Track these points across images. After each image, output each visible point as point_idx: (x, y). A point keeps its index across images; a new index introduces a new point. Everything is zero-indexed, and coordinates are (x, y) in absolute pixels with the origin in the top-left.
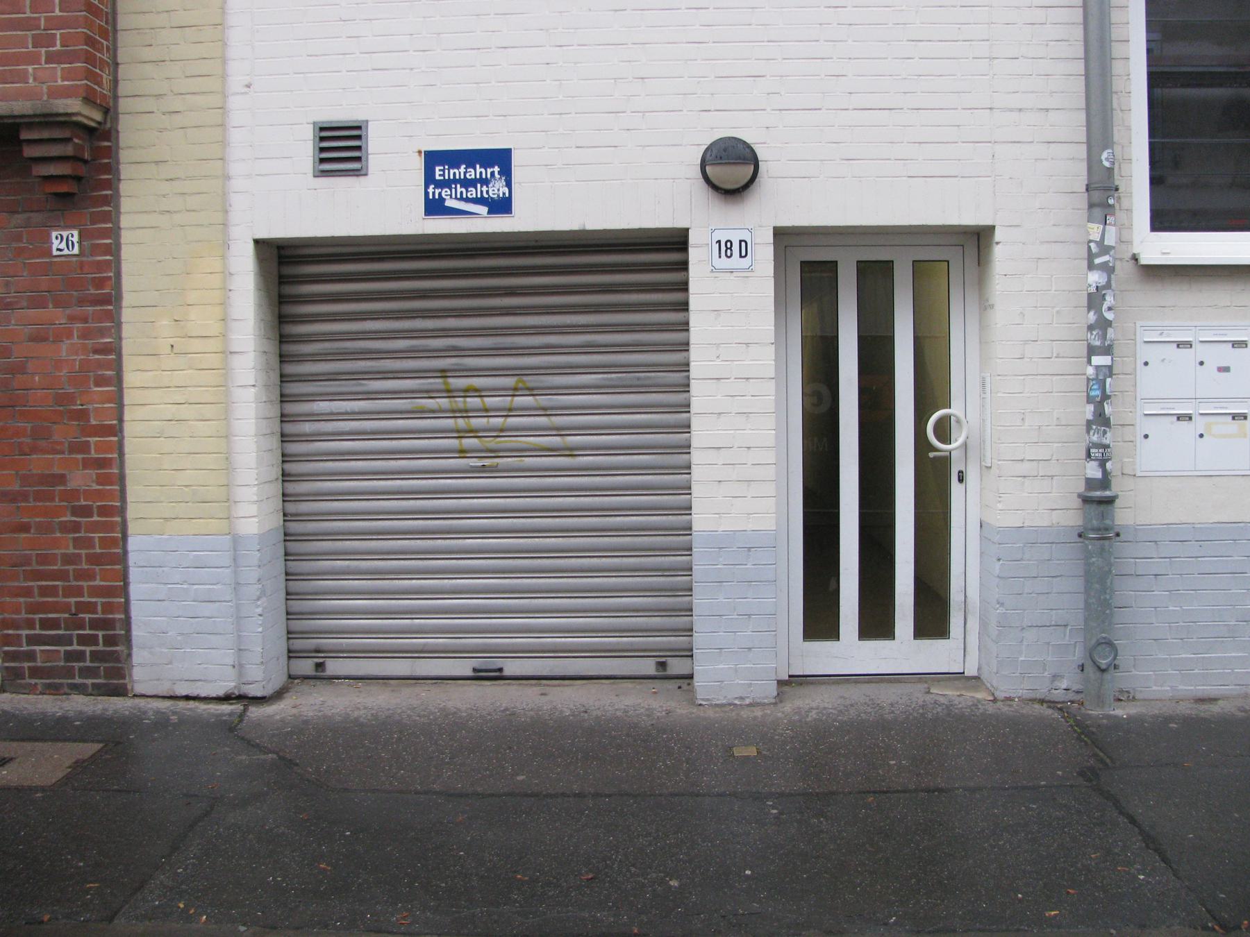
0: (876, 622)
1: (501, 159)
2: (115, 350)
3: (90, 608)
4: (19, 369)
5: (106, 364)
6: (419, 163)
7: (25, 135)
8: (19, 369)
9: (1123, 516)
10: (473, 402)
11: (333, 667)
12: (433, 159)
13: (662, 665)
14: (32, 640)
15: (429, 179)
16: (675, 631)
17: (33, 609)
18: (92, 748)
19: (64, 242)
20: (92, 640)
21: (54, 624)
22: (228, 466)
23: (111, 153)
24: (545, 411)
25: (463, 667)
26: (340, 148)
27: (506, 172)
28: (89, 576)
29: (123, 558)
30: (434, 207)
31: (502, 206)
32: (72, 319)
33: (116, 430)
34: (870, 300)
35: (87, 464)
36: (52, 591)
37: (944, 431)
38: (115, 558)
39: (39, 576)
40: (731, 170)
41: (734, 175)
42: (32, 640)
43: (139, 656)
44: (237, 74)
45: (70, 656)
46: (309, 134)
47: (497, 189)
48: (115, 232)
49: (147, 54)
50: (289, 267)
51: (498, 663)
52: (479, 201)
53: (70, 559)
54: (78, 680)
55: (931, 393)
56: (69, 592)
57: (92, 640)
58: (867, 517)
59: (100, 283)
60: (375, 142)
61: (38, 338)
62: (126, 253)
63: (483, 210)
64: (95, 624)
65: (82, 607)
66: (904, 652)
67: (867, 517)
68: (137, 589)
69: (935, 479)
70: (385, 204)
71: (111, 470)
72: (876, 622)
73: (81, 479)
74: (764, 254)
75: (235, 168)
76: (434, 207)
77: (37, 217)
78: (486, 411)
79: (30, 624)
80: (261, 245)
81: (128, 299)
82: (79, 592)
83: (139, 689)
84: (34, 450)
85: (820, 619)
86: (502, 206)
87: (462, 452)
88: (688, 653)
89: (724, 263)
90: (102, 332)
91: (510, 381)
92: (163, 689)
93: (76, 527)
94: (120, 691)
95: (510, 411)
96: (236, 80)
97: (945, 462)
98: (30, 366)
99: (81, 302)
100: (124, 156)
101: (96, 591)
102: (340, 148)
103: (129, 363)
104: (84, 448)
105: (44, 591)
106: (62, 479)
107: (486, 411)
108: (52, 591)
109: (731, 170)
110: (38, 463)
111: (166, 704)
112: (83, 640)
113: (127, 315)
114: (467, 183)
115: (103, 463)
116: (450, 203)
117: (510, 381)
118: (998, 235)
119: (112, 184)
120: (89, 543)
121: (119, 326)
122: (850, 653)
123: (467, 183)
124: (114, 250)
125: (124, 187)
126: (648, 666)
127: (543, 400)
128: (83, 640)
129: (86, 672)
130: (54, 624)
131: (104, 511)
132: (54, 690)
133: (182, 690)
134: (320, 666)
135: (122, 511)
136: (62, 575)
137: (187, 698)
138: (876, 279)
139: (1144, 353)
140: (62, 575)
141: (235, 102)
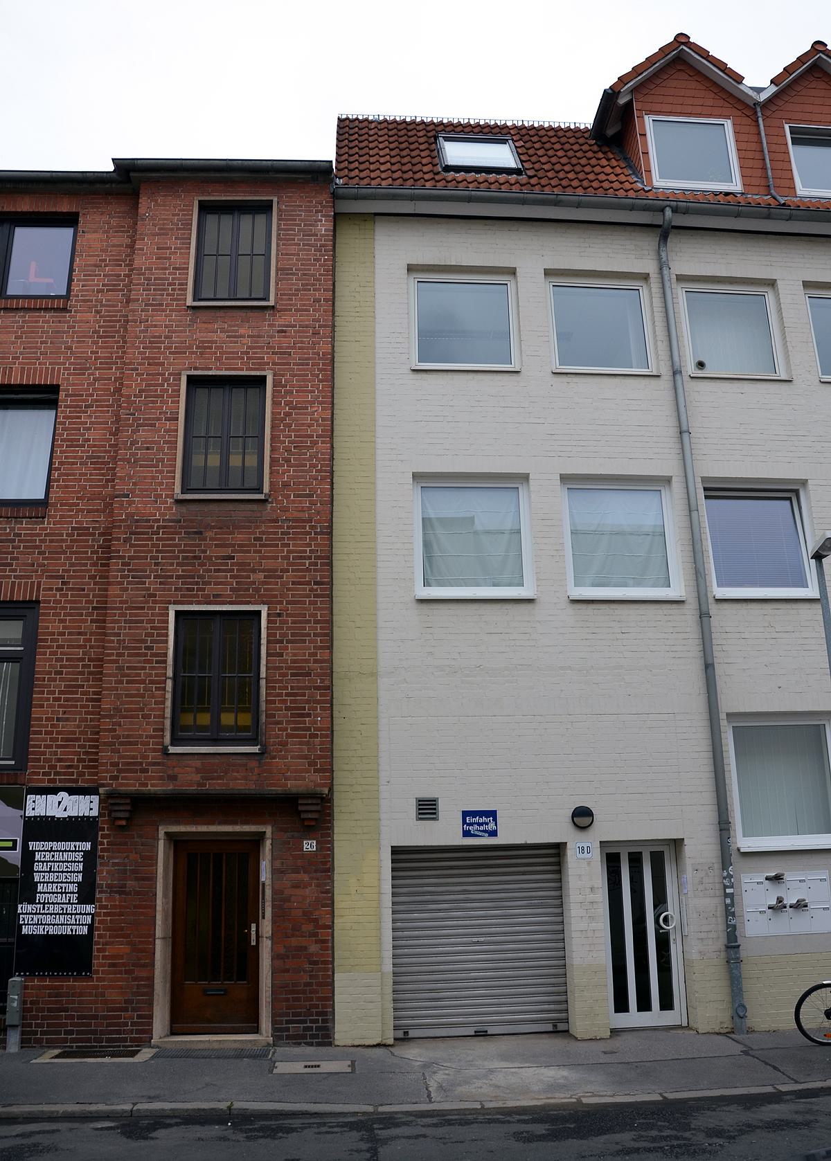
0: (644, 1005)
1: (492, 814)
3: (317, 1006)
4: (288, 900)
5: (327, 899)
8: (288, 900)
9: (743, 953)
11: (412, 1034)
12: (466, 814)
13: (555, 1026)
14: (288, 1022)
15: (464, 822)
16: (560, 1011)
19: (310, 846)
20: (316, 1021)
21: (299, 1014)
22: (380, 943)
23: (331, 808)
25: (471, 1031)
27: (495, 820)
30: (466, 834)
31: (493, 833)
32: (312, 879)
33: (331, 927)
34: (637, 869)
35: (316, 942)
36: (298, 999)
37: (666, 920)
39: (293, 992)
40: (582, 817)
41: (583, 821)
42: (288, 1022)
43: (338, 1027)
44: (384, 776)
45: (305, 1029)
47: (491, 826)
48: (332, 842)
49: (346, 767)
50: (406, 859)
51: (486, 1028)
52: (485, 831)
55: (660, 899)
56: (307, 999)
57: (316, 1021)
58: (642, 969)
59: (325, 863)
60: (441, 806)
61: (296, 886)
64: (318, 1014)
65: (312, 1006)
66: (656, 1017)
67: (642, 969)
69: (663, 943)
70: (446, 831)
71: (327, 944)
72: (644, 1005)
73: (314, 948)
75: (383, 816)
76: (466, 834)
77: (296, 834)
79: (287, 1015)
80: (395, 851)
84: (293, 936)
85: (621, 1005)
86: (493, 833)
88: (567, 1021)
90: (326, 884)
92: (349, 1042)
96: (383, 780)
97: (667, 934)
98: (293, 899)
99: (316, 871)
100: (336, 810)
101: (319, 999)
102: (427, 809)
104: (316, 935)
105: (295, 999)
108: (298, 999)
109: (582, 817)
110: (294, 942)
112: (312, 1021)
114: (479, 824)
118: (686, 842)
119: (331, 821)
120: (317, 977)
121: (333, 882)
122: (634, 1018)
123: (479, 824)
124: (332, 849)
126: (549, 1027)
128: (312, 1021)
129: (312, 1036)
130: (299, 1014)
131: (323, 962)
134: (406, 1033)
135: (333, 962)
136: (304, 992)
138: (636, 860)
139: (744, 887)
140: (304, 992)
141: (382, 788)
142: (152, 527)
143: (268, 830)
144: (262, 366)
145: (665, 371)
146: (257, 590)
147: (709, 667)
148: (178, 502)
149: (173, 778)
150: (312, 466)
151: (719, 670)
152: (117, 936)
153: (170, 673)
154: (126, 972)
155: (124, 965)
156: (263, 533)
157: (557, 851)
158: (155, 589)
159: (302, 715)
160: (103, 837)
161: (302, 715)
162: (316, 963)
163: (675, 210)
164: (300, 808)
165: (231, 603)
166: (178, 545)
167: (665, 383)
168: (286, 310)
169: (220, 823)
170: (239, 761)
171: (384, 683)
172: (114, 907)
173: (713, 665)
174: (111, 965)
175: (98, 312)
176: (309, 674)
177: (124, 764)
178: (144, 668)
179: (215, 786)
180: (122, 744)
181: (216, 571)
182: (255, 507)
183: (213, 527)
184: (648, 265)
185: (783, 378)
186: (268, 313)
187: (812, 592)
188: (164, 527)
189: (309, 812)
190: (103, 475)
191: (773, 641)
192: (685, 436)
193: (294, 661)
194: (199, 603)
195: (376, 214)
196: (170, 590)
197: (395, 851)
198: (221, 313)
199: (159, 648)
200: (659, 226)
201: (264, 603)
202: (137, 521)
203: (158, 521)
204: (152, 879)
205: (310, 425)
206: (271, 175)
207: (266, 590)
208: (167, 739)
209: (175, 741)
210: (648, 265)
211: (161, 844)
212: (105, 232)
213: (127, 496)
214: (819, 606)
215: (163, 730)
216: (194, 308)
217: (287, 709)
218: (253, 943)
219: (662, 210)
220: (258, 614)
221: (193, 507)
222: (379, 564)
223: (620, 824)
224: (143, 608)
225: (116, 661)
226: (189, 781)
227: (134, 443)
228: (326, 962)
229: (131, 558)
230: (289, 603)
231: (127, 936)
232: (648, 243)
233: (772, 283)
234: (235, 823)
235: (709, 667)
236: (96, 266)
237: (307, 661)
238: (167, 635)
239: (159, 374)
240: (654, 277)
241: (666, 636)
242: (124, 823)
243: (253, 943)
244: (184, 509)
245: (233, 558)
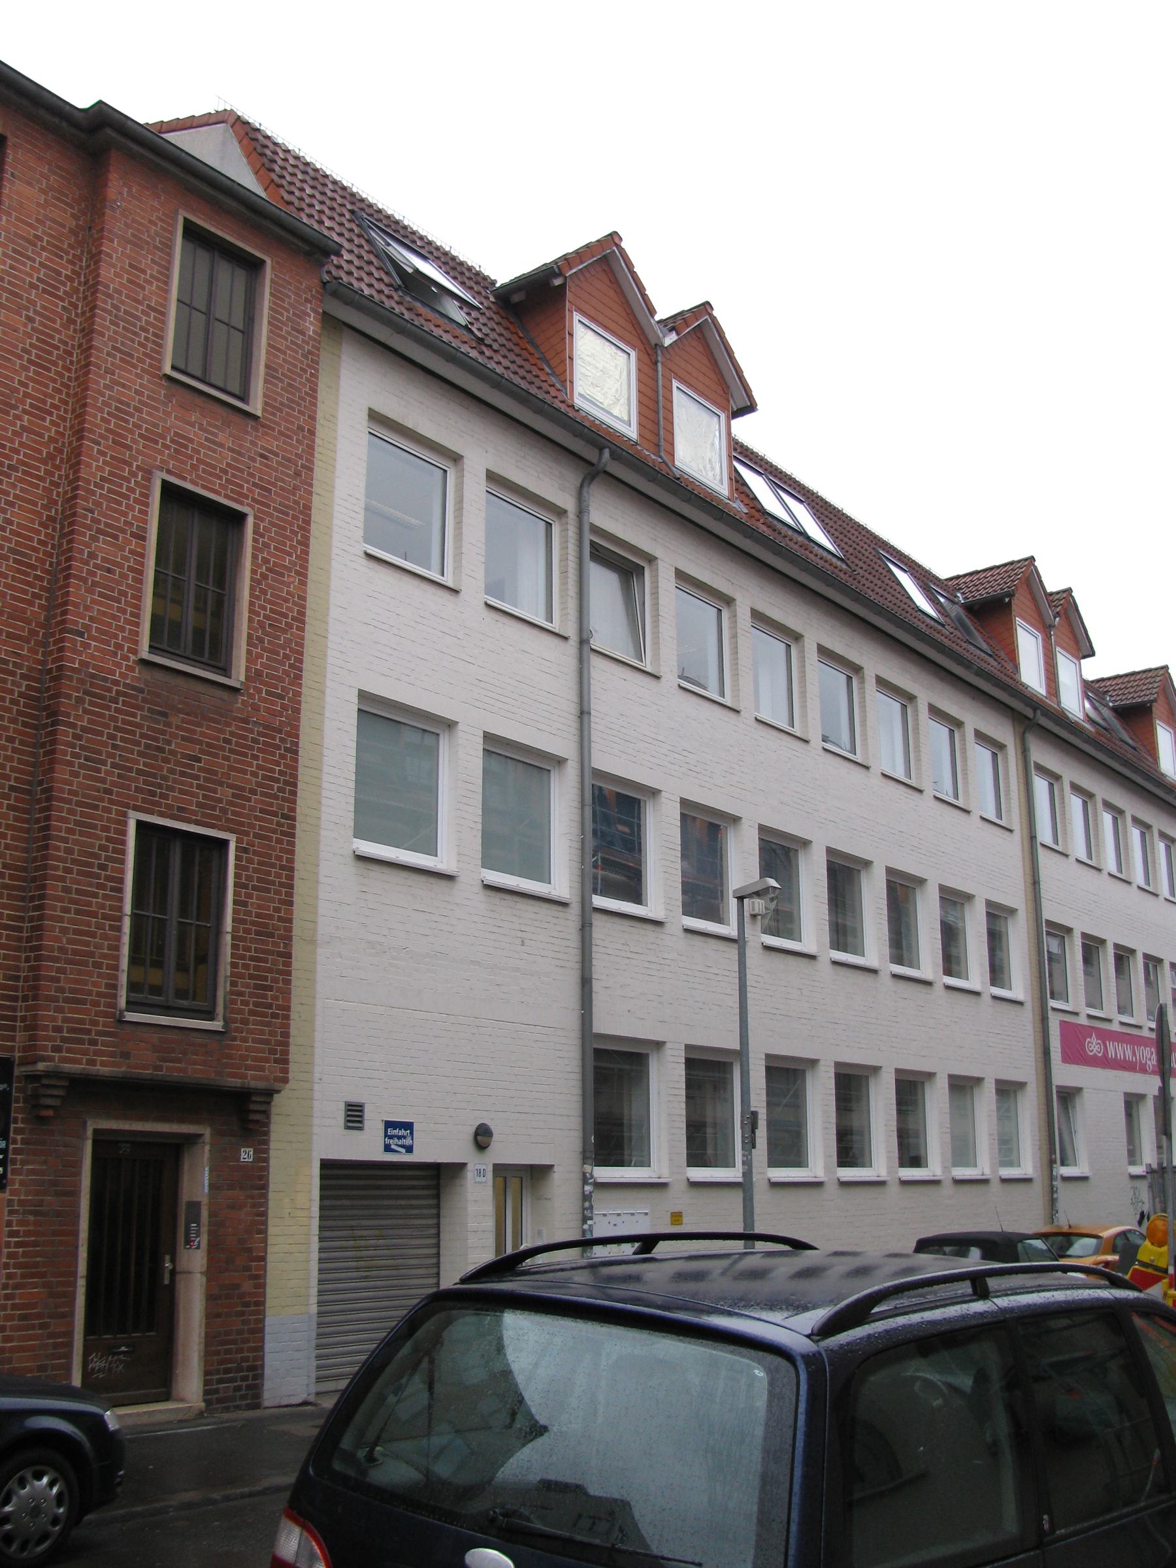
1: (409, 1126)
2: (264, 1214)
6: (382, 1126)
7: (254, 1099)
10: (363, 1243)
12: (389, 1125)
17: (221, 1362)
18: (876, 1310)
19: (246, 1155)
21: (227, 1371)
24: (388, 1247)
26: (354, 1115)
27: (412, 1133)
28: (248, 1341)
29: (262, 1330)
30: (388, 1148)
31: (409, 1149)
33: (263, 1259)
38: (258, 1330)
40: (482, 1137)
43: (268, 1385)
46: (342, 1107)
47: (408, 1142)
50: (336, 1173)
52: (402, 1146)
53: (240, 1332)
54: (238, 1403)
61: (232, 1207)
62: (272, 1162)
63: (403, 1150)
68: (269, 1346)
70: (367, 1146)
71: (259, 1281)
73: (247, 1286)
74: (490, 1175)
76: (388, 1148)
78: (367, 1248)
80: (326, 1165)
81: (272, 1187)
82: (240, 1350)
83: (266, 1403)
87: (357, 1269)
89: (478, 1179)
90: (261, 1205)
91: (376, 1232)
93: (242, 1313)
94: (257, 1406)
95: (376, 1247)
102: (354, 1115)
103: (271, 1222)
104: (248, 1269)
106: (237, 1286)
107: (367, 1248)
109: (482, 1137)
111: (276, 1410)
113: (271, 1195)
114: (399, 1138)
115: (257, 1277)
116: (393, 1147)
117: (376, 1232)
123: (399, 1138)
125: (273, 1127)
127: (388, 1242)
129: (243, 1398)
132: (227, 1409)
133: (285, 1402)
135: (263, 1303)
137: (287, 1406)
142: (109, 690)
143: (206, 1131)
144: (240, 497)
145: (571, 631)
146: (224, 811)
147: (586, 982)
148: (144, 663)
149: (126, 1055)
150: (286, 657)
151: (596, 986)
152: (33, 1276)
153: (128, 908)
154: (41, 1326)
155: (39, 1316)
156: (232, 734)
157: (457, 1169)
158: (113, 784)
159: (265, 988)
160: (18, 1131)
161: (265, 988)
162: (247, 1305)
163: (612, 454)
164: (253, 1107)
165: (197, 823)
166: (140, 726)
167: (571, 647)
168: (270, 428)
169: (117, 1118)
170: (199, 1039)
171: (322, 953)
172: (28, 1234)
173: (591, 979)
174: (23, 1317)
175: (30, 319)
176: (272, 935)
177: (71, 1030)
178: (95, 895)
179: (170, 1071)
180: (66, 1000)
181: (183, 774)
182: (225, 695)
183: (180, 711)
184: (567, 501)
185: (648, 669)
186: (251, 423)
187: (730, 930)
188: (125, 694)
189: (243, 1111)
190: (28, 583)
191: (627, 961)
192: (585, 717)
193: (258, 915)
194: (161, 815)
195: (345, 324)
196: (128, 788)
197: (326, 1165)
198: (199, 400)
199: (114, 869)
200: (593, 465)
201: (232, 831)
202: (93, 676)
203: (117, 683)
204: (75, 1194)
205: (286, 600)
206: (267, 223)
207: (234, 813)
208: (122, 1002)
209: (132, 1005)
210: (567, 501)
211: (89, 1145)
212: (42, 191)
213: (81, 635)
214: (736, 946)
215: (115, 987)
216: (169, 378)
217: (251, 977)
218: (167, 1281)
219: (601, 449)
220: (224, 843)
221: (159, 675)
222: (324, 801)
223: (509, 1149)
224: (96, 807)
225: (62, 879)
226: (144, 1064)
227: (92, 556)
228: (258, 1304)
229: (84, 729)
230: (256, 836)
231: (42, 1275)
232: (573, 478)
233: (456, 459)
234: (143, 1118)
235: (586, 982)
236: (28, 241)
237: (271, 917)
238: (123, 852)
239: (125, 462)
240: (572, 515)
241: (727, 973)
242: (50, 1113)
243: (167, 1281)
244: (147, 675)
245: (199, 760)
